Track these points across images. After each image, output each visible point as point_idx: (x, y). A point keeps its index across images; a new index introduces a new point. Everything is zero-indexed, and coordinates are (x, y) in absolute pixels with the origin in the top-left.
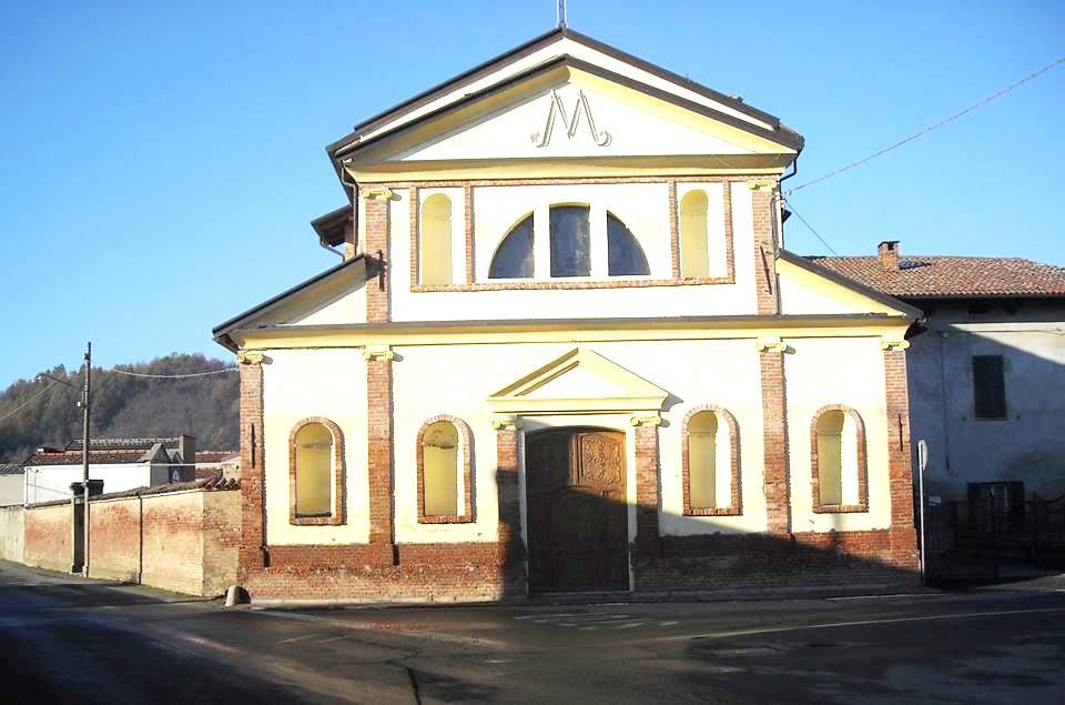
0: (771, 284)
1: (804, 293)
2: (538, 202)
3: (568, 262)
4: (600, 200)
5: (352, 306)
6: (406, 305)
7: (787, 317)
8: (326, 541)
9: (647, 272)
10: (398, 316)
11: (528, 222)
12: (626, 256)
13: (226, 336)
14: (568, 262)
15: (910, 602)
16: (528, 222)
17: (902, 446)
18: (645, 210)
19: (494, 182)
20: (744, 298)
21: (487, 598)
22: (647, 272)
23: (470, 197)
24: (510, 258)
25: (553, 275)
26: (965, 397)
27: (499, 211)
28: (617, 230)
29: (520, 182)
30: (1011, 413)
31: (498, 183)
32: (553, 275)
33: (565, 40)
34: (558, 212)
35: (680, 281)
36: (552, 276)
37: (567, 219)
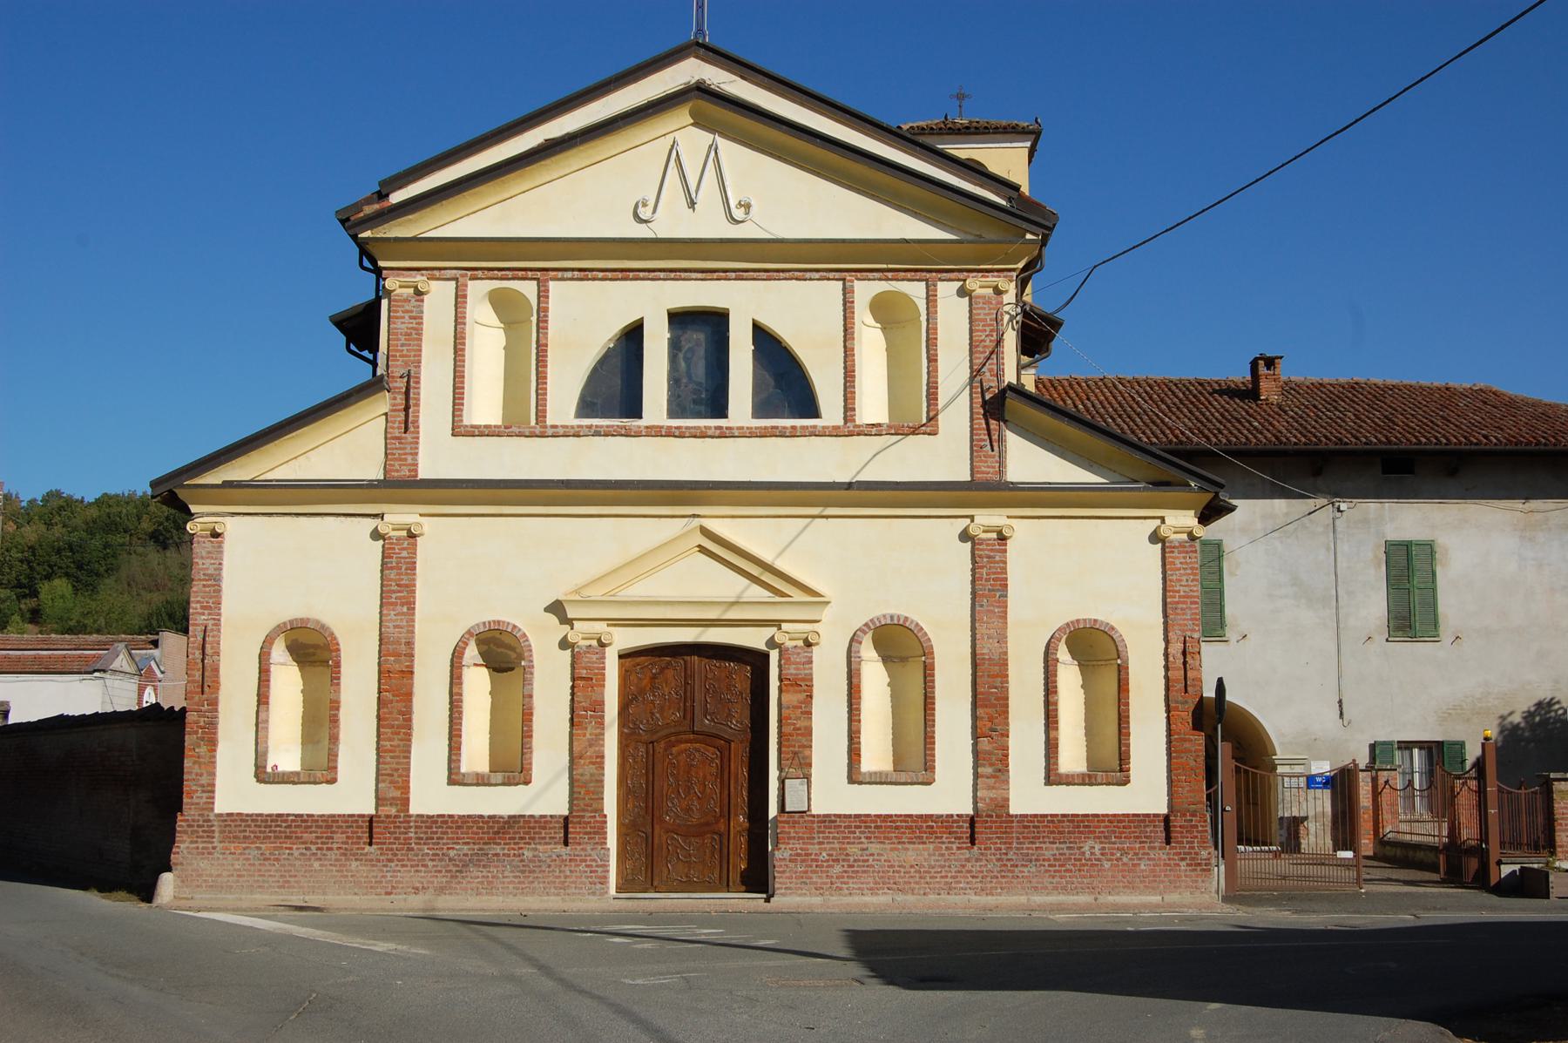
0: (985, 443)
1: (1027, 461)
2: (653, 302)
3: (703, 396)
4: (747, 303)
5: (350, 447)
7: (1014, 487)
10: (429, 467)
11: (633, 335)
12: (787, 386)
13: (172, 494)
16: (633, 335)
17: (371, 828)
18: (803, 313)
19: (585, 274)
20: (945, 455)
23: (543, 295)
24: (615, 389)
25: (672, 414)
26: (1373, 605)
27: (586, 318)
28: (773, 353)
29: (625, 274)
30: (1230, 634)
31: (590, 275)
32: (672, 414)
34: (679, 319)
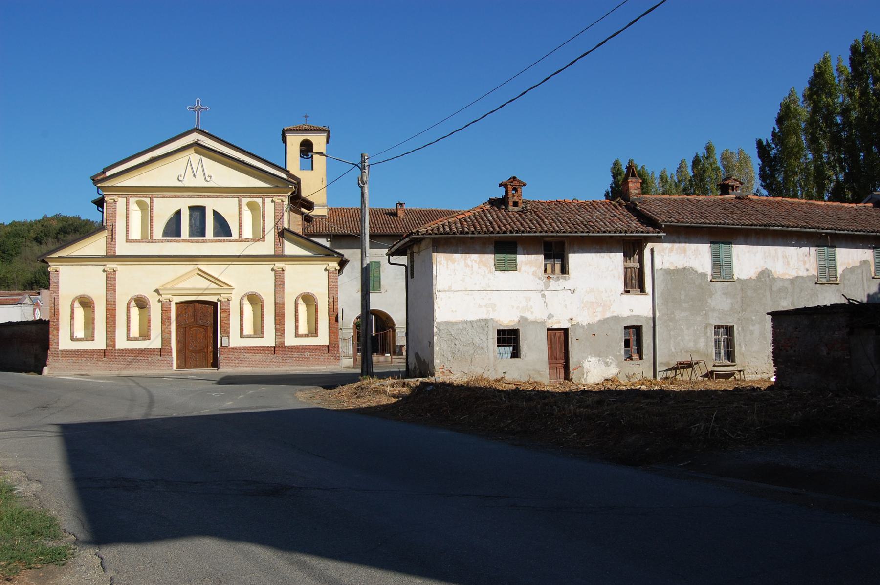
2: (183, 204)
3: (198, 230)
4: (211, 204)
6: (122, 248)
8: (143, 347)
9: (231, 236)
10: (118, 252)
11: (178, 213)
12: (223, 228)
14: (198, 230)
15: (64, 373)
16: (178, 213)
18: (227, 207)
20: (267, 247)
21: (385, 401)
22: (231, 236)
23: (152, 202)
24: (173, 229)
27: (164, 209)
28: (219, 219)
32: (190, 236)
33: (195, 134)
34: (191, 208)
35: (240, 240)
36: (379, 263)
37: (198, 212)
